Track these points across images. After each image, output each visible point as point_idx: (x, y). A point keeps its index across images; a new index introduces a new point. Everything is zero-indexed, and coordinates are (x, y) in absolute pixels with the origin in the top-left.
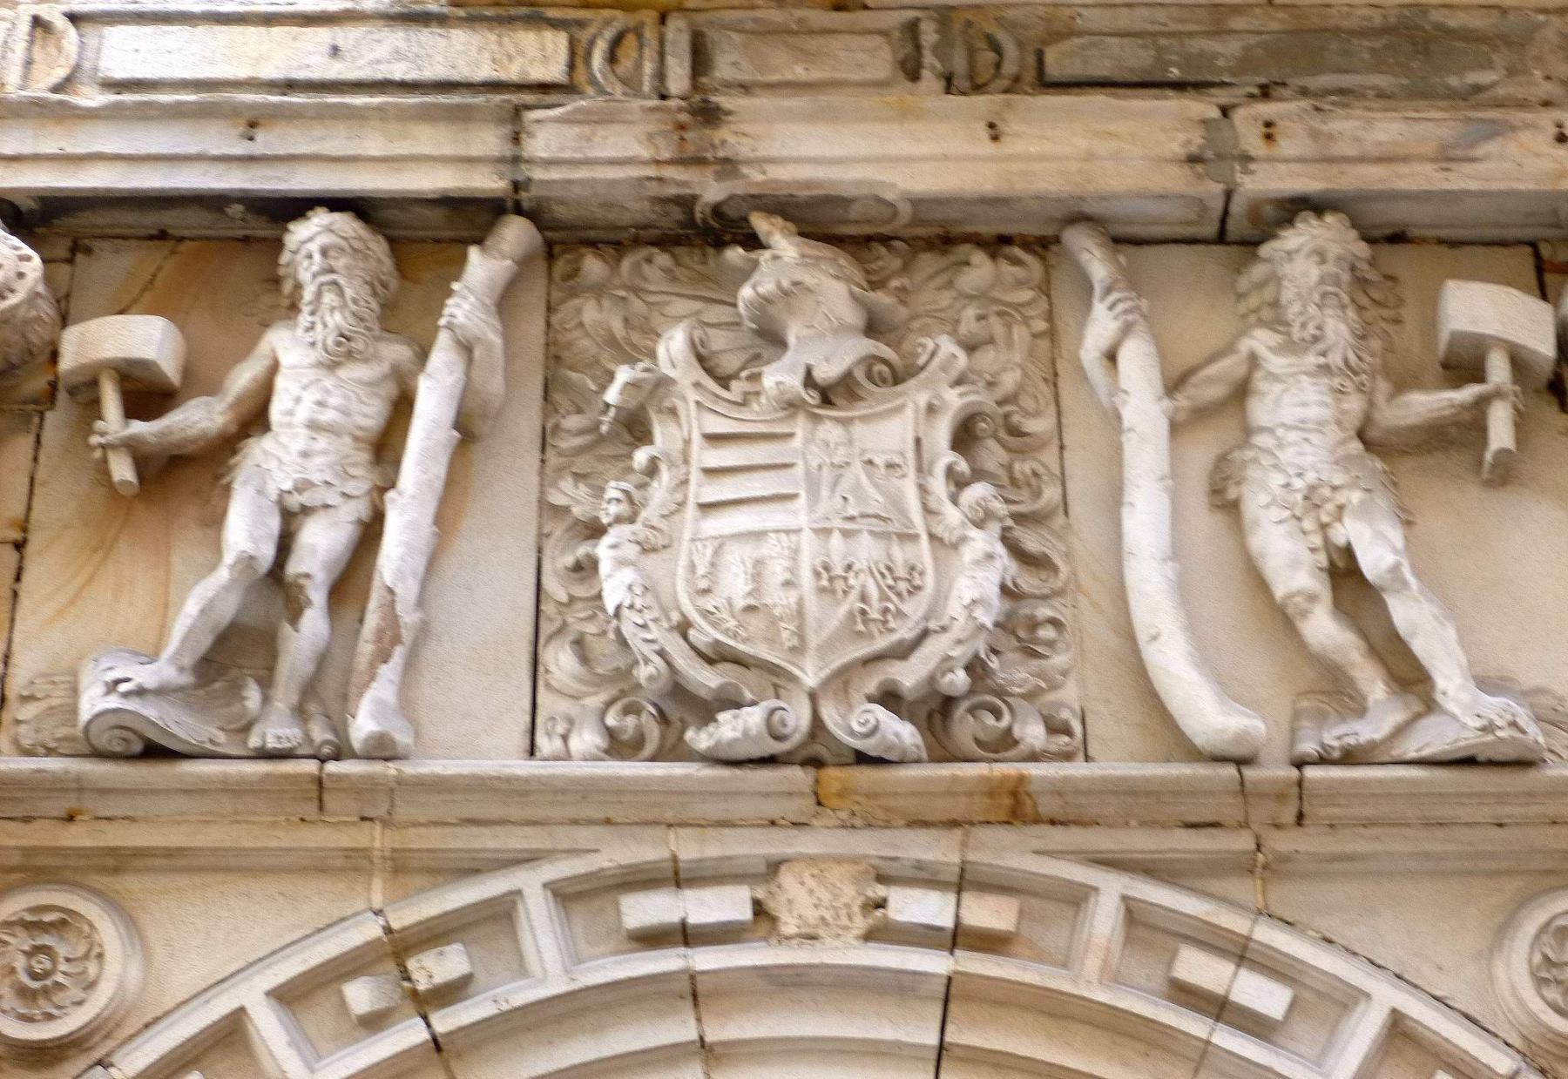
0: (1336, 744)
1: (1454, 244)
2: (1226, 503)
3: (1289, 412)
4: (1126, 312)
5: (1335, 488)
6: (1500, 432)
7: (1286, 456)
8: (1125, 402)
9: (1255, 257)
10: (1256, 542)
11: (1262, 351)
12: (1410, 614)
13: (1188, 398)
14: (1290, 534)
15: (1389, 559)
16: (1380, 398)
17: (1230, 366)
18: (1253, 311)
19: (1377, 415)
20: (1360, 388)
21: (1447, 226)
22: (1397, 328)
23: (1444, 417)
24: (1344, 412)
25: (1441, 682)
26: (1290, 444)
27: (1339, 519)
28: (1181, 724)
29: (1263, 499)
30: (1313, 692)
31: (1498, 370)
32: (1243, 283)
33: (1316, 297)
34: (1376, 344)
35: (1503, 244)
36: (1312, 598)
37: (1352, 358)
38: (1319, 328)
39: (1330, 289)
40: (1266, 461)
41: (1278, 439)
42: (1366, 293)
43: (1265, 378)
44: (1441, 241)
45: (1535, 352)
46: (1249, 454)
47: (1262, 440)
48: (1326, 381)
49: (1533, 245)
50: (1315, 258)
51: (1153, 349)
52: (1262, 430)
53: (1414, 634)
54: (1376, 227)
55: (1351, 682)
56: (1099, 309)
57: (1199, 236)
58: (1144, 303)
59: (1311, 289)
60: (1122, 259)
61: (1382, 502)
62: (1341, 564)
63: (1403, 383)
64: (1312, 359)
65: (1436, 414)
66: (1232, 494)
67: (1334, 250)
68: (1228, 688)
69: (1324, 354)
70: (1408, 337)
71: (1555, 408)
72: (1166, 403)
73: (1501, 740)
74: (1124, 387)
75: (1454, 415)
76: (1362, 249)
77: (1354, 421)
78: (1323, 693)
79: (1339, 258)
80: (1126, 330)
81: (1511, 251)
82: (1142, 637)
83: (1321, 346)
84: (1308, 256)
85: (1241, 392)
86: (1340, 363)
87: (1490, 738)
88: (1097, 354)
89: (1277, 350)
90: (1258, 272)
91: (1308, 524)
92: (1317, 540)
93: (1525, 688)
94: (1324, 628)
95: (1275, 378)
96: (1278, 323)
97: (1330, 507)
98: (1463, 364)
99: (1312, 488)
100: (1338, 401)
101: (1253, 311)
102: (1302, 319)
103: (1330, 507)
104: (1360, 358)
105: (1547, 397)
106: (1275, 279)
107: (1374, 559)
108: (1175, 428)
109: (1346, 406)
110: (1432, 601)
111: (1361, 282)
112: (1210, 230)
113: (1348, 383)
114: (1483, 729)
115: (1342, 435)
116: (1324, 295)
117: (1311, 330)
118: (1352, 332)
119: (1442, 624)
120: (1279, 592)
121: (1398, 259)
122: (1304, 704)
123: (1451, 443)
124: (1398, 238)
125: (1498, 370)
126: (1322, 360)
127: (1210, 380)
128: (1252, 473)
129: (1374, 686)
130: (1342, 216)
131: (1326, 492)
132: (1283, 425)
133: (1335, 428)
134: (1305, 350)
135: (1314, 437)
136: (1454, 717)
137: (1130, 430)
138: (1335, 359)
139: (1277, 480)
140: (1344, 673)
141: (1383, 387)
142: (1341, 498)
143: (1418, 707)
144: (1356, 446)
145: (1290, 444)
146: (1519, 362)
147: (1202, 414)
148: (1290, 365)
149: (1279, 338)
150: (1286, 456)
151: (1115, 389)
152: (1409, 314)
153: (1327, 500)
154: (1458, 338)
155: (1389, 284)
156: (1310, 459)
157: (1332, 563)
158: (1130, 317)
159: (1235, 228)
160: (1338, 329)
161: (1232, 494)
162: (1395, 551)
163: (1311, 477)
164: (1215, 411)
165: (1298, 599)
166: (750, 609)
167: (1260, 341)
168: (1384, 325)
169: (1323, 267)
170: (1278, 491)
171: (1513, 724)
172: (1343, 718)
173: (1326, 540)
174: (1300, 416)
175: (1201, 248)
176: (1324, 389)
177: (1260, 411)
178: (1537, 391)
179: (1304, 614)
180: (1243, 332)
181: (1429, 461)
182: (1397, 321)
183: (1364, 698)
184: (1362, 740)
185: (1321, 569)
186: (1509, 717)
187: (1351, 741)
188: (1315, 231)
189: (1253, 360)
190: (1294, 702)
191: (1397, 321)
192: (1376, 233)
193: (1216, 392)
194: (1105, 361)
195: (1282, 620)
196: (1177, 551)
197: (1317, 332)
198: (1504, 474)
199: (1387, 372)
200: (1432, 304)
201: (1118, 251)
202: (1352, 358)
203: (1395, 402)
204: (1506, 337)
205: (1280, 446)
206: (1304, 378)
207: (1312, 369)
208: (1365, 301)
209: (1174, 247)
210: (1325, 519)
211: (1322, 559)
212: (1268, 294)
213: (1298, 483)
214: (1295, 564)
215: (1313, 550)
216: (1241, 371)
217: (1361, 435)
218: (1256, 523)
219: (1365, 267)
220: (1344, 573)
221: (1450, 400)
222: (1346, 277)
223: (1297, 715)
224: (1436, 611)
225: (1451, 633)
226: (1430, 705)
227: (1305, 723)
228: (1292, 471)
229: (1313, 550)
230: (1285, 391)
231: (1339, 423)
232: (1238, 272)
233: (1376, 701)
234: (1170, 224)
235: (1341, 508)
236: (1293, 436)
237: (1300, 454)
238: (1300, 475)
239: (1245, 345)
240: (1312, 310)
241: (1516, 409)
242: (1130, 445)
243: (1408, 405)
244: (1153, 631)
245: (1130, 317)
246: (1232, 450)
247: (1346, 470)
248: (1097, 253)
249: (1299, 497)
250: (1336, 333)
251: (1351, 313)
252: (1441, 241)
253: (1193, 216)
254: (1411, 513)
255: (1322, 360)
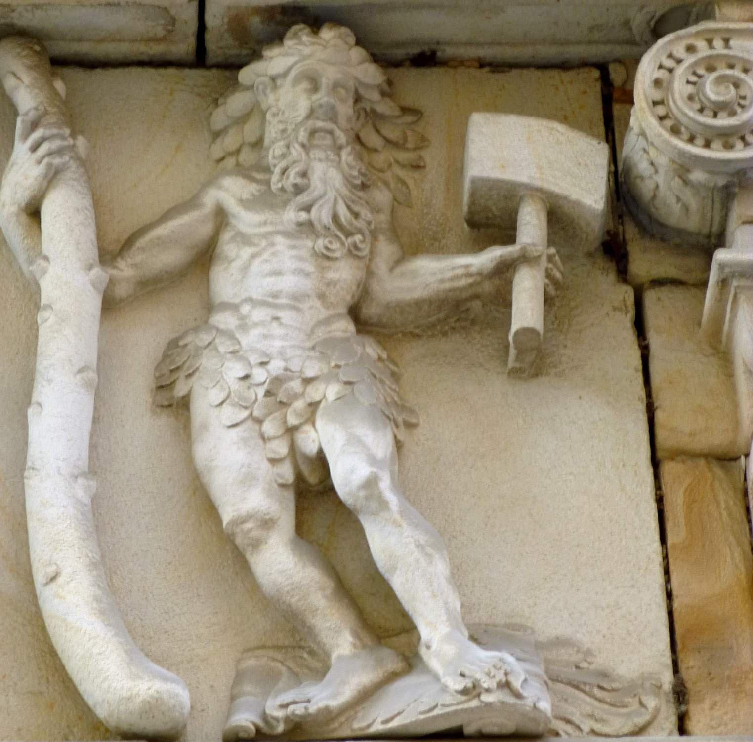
0: (280, 714)
1: (498, 66)
2: (173, 403)
3: (258, 284)
4: (50, 154)
5: (308, 381)
6: (526, 308)
7: (248, 340)
8: (44, 272)
9: (234, 85)
10: (202, 452)
11: (232, 205)
12: (394, 544)
13: (135, 266)
14: (245, 441)
15: (364, 471)
16: (381, 266)
17: (192, 225)
18: (231, 154)
19: (375, 286)
20: (353, 252)
21: (491, 44)
22: (417, 175)
23: (462, 289)
24: (330, 284)
25: (425, 632)
26: (256, 325)
27: (311, 419)
28: (81, 689)
29: (215, 395)
30: (263, 647)
31: (531, 227)
32: (219, 118)
33: (303, 135)
34: (382, 196)
35: (564, 66)
36: (267, 523)
37: (343, 211)
38: (304, 174)
39: (320, 124)
40: (224, 346)
41: (243, 318)
42: (378, 131)
43: (233, 239)
44: (482, 64)
45: (577, 204)
46: (205, 338)
47: (224, 320)
48: (309, 243)
49: (603, 68)
50: (305, 85)
51: (87, 202)
52: (226, 306)
53: (394, 569)
54: (398, 45)
55: (311, 632)
56: (21, 149)
57: (169, 57)
58: (81, 142)
59: (298, 126)
60: (59, 85)
61: (367, 395)
62: (312, 479)
63: (412, 246)
64: (291, 215)
65: (447, 286)
66: (180, 390)
67: (330, 75)
68: (143, 641)
69: (308, 209)
70: (429, 187)
71: (612, 277)
72: (97, 271)
73: (488, 705)
74: (45, 251)
75: (471, 285)
76: (371, 74)
77: (344, 295)
78: (277, 648)
79: (336, 86)
80: (52, 177)
81: (572, 74)
82: (39, 578)
83: (304, 198)
84: (296, 81)
85: (205, 257)
86: (326, 219)
87: (474, 703)
88: (14, 209)
89: (247, 204)
90: (236, 102)
91: (270, 427)
92: (281, 448)
93: (542, 638)
94: (280, 563)
95: (244, 239)
96: (254, 171)
97: (299, 404)
98: (491, 221)
99: (278, 380)
100: (322, 269)
101: (231, 154)
102: (283, 164)
103: (299, 404)
104: (356, 215)
105: (601, 261)
106: (256, 112)
107: (348, 474)
108: (110, 305)
109: (331, 275)
110: (417, 526)
111: (371, 117)
112: (185, 47)
113: (336, 245)
114: (465, 692)
115: (324, 313)
116: (313, 133)
117: (293, 177)
118: (347, 179)
119: (429, 556)
120: (227, 515)
121: (420, 87)
122: (250, 662)
123: (473, 322)
124: (426, 59)
125: (531, 227)
126: (303, 216)
127: (162, 243)
128: (207, 362)
129: (340, 638)
130: (344, 30)
131: (296, 385)
132: (249, 300)
133: (318, 304)
134: (285, 204)
135: (286, 316)
136: (437, 678)
137: (49, 306)
138: (322, 215)
139: (235, 370)
140: (304, 623)
141: (386, 250)
142: (314, 393)
143: (393, 663)
144: (346, 327)
145: (256, 325)
146: (559, 218)
147: (152, 286)
148: (265, 223)
149: (253, 188)
150: (248, 340)
151: (36, 252)
152: (433, 157)
153: (296, 397)
154: (483, 186)
155: (409, 119)
156: (278, 343)
157: (300, 478)
158: (57, 161)
159: (218, 44)
160: (328, 177)
161: (180, 390)
162: (372, 460)
163: (276, 366)
164: (161, 283)
165: (249, 525)
166: (695, 638)
167: (231, 191)
168: (402, 173)
169: (315, 97)
170: (235, 385)
171: (506, 685)
172: (297, 679)
173: (293, 448)
174: (273, 291)
175: (171, 71)
176: (305, 253)
177: (225, 282)
178: (590, 255)
179: (256, 544)
180: (211, 182)
181: (444, 345)
182: (417, 167)
183: (328, 655)
184: (313, 709)
185: (283, 486)
186: (500, 676)
187: (299, 710)
188: (307, 51)
189: (221, 217)
190: (238, 661)
191: (417, 167)
192: (399, 53)
193: (171, 258)
194: (24, 218)
195: (229, 551)
196: (98, 461)
197: (299, 180)
198: (534, 361)
199: (395, 232)
200: (458, 141)
201: (54, 74)
202: (343, 211)
203: (398, 271)
204: (546, 186)
205: (244, 327)
206: (279, 239)
207: (292, 227)
208: (373, 140)
209: (135, 71)
210: (292, 420)
211: (287, 473)
212: (250, 131)
213: (260, 375)
214: (248, 480)
215: (273, 461)
216: (206, 230)
217: (355, 313)
218: (205, 427)
219: (375, 96)
220: (311, 491)
221: (467, 266)
222: (345, 110)
223: (239, 677)
224: (423, 539)
225: (441, 568)
226: (411, 660)
227: (248, 688)
228: (254, 359)
229: (273, 461)
230: (253, 256)
231: (322, 297)
232: (216, 103)
233: (340, 657)
234: (133, 41)
235: (314, 406)
236: (259, 314)
237: (265, 337)
238: (263, 364)
239: (210, 198)
240: (296, 151)
241: (549, 276)
242: (47, 322)
243: (414, 274)
244: (52, 570)
245: (57, 161)
246: (185, 334)
247: (324, 357)
248: (27, 78)
249: (261, 392)
250: (324, 181)
251: (346, 156)
252: (482, 64)
253: (160, 32)
254: (411, 411)
255: (303, 216)
